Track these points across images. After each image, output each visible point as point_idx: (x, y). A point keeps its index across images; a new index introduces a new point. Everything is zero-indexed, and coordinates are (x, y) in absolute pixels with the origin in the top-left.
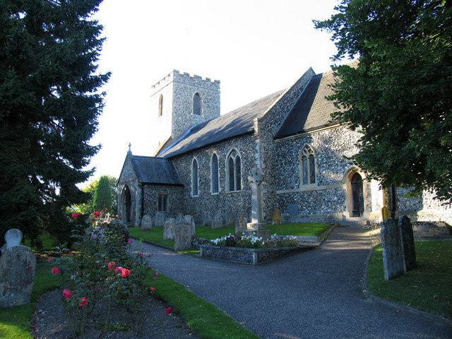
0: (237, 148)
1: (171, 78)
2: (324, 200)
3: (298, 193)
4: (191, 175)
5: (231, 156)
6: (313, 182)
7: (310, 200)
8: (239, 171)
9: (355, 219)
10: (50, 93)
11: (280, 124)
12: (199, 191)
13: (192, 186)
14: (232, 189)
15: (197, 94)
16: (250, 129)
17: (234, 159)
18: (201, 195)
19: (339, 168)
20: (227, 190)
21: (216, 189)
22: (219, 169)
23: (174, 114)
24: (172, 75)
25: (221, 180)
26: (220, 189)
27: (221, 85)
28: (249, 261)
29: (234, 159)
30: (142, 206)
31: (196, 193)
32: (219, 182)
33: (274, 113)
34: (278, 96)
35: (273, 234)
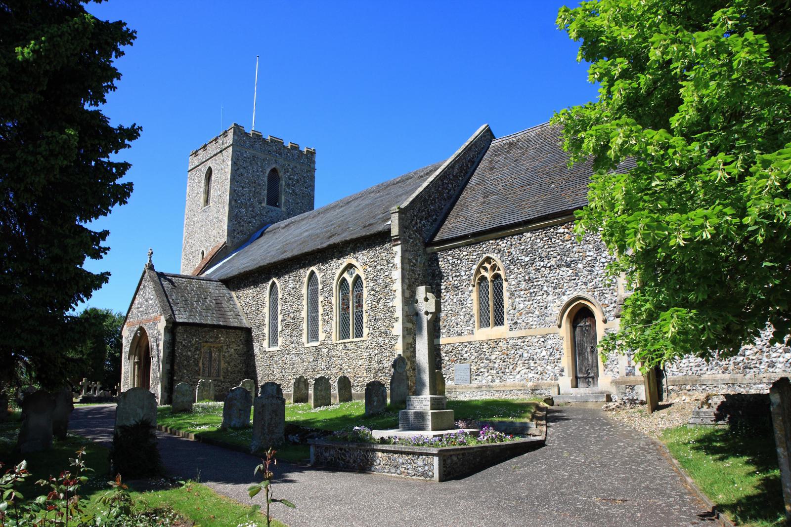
0: (360, 261)
1: (230, 139)
2: (521, 356)
3: (470, 343)
4: (266, 310)
5: (346, 275)
6: (499, 321)
7: (493, 357)
8: (359, 304)
9: (583, 390)
10: (26, 61)
11: (436, 220)
12: (280, 340)
13: (266, 330)
14: (344, 334)
15: (274, 171)
16: (380, 228)
17: (350, 280)
18: (286, 348)
19: (550, 298)
20: (334, 338)
21: (314, 335)
22: (321, 299)
23: (233, 203)
24: (231, 134)
25: (324, 320)
26: (322, 336)
27: (318, 158)
28: (424, 474)
29: (350, 280)
30: (172, 366)
31: (274, 341)
32: (320, 323)
33: (425, 200)
34: (422, 178)
35: (726, 416)
